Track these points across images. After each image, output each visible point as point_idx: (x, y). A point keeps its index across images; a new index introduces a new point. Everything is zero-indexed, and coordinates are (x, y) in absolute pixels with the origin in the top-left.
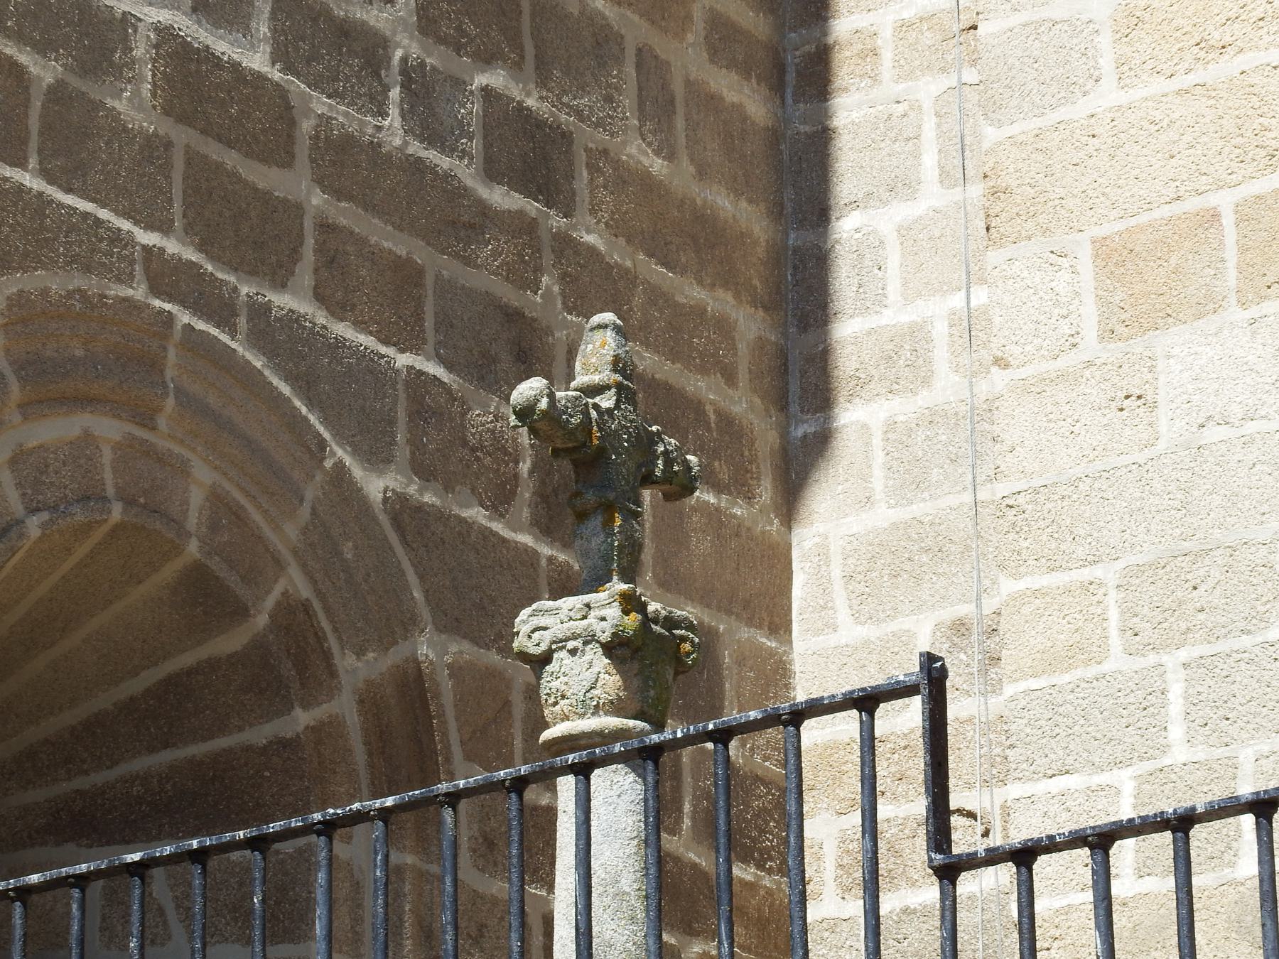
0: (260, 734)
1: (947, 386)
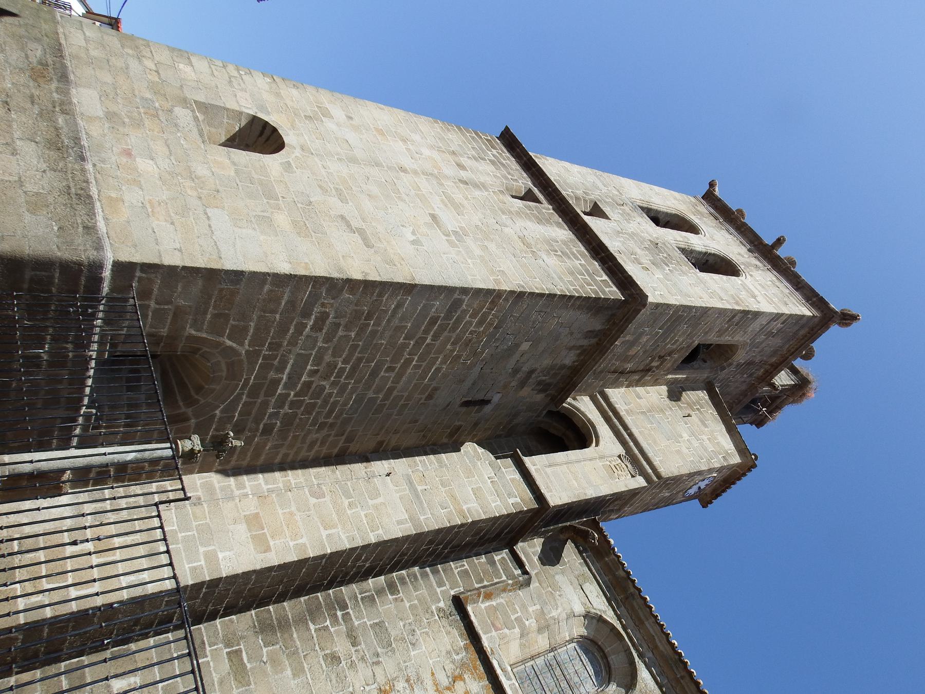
0: (179, 398)
1: (237, 493)
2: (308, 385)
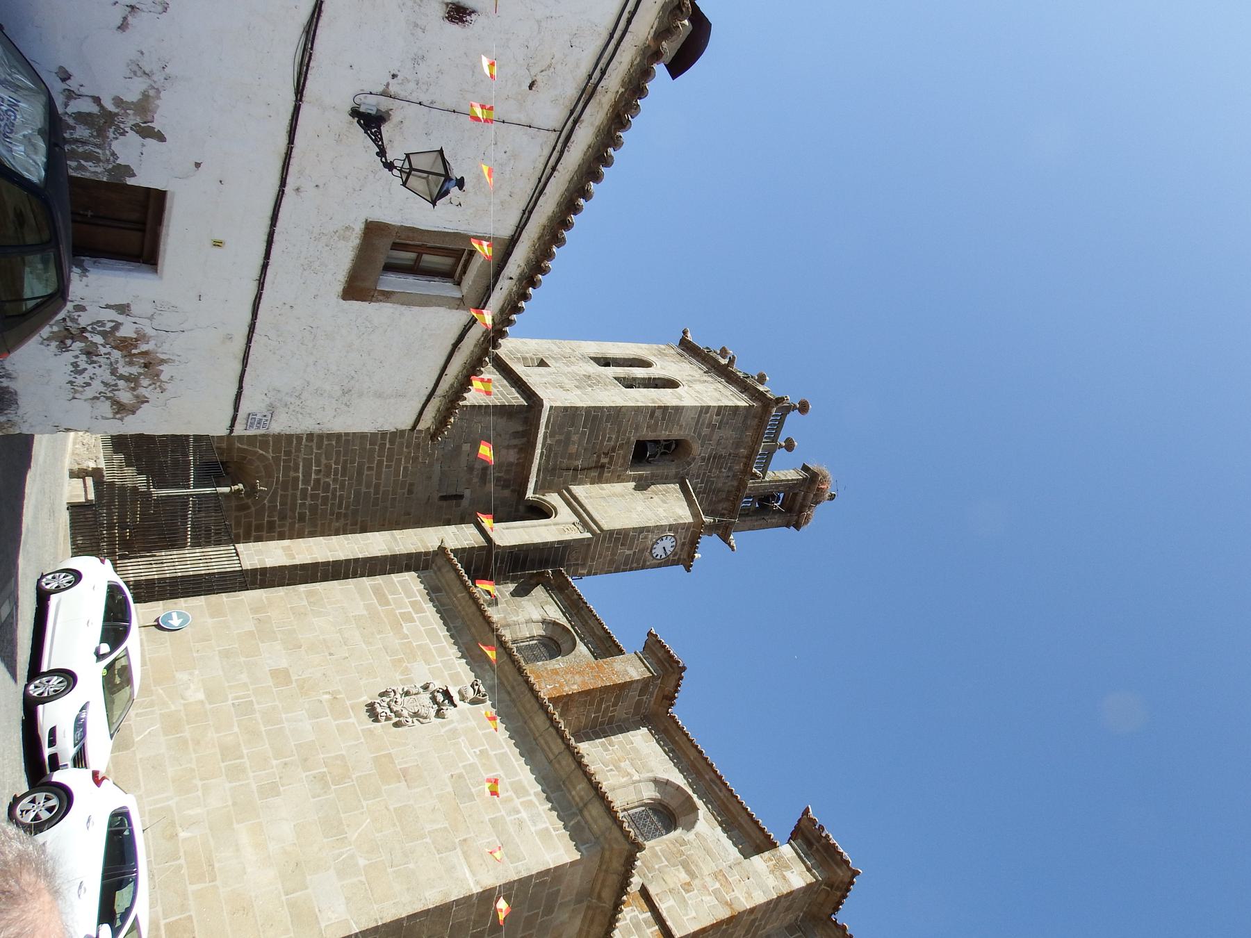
2: (317, 481)
